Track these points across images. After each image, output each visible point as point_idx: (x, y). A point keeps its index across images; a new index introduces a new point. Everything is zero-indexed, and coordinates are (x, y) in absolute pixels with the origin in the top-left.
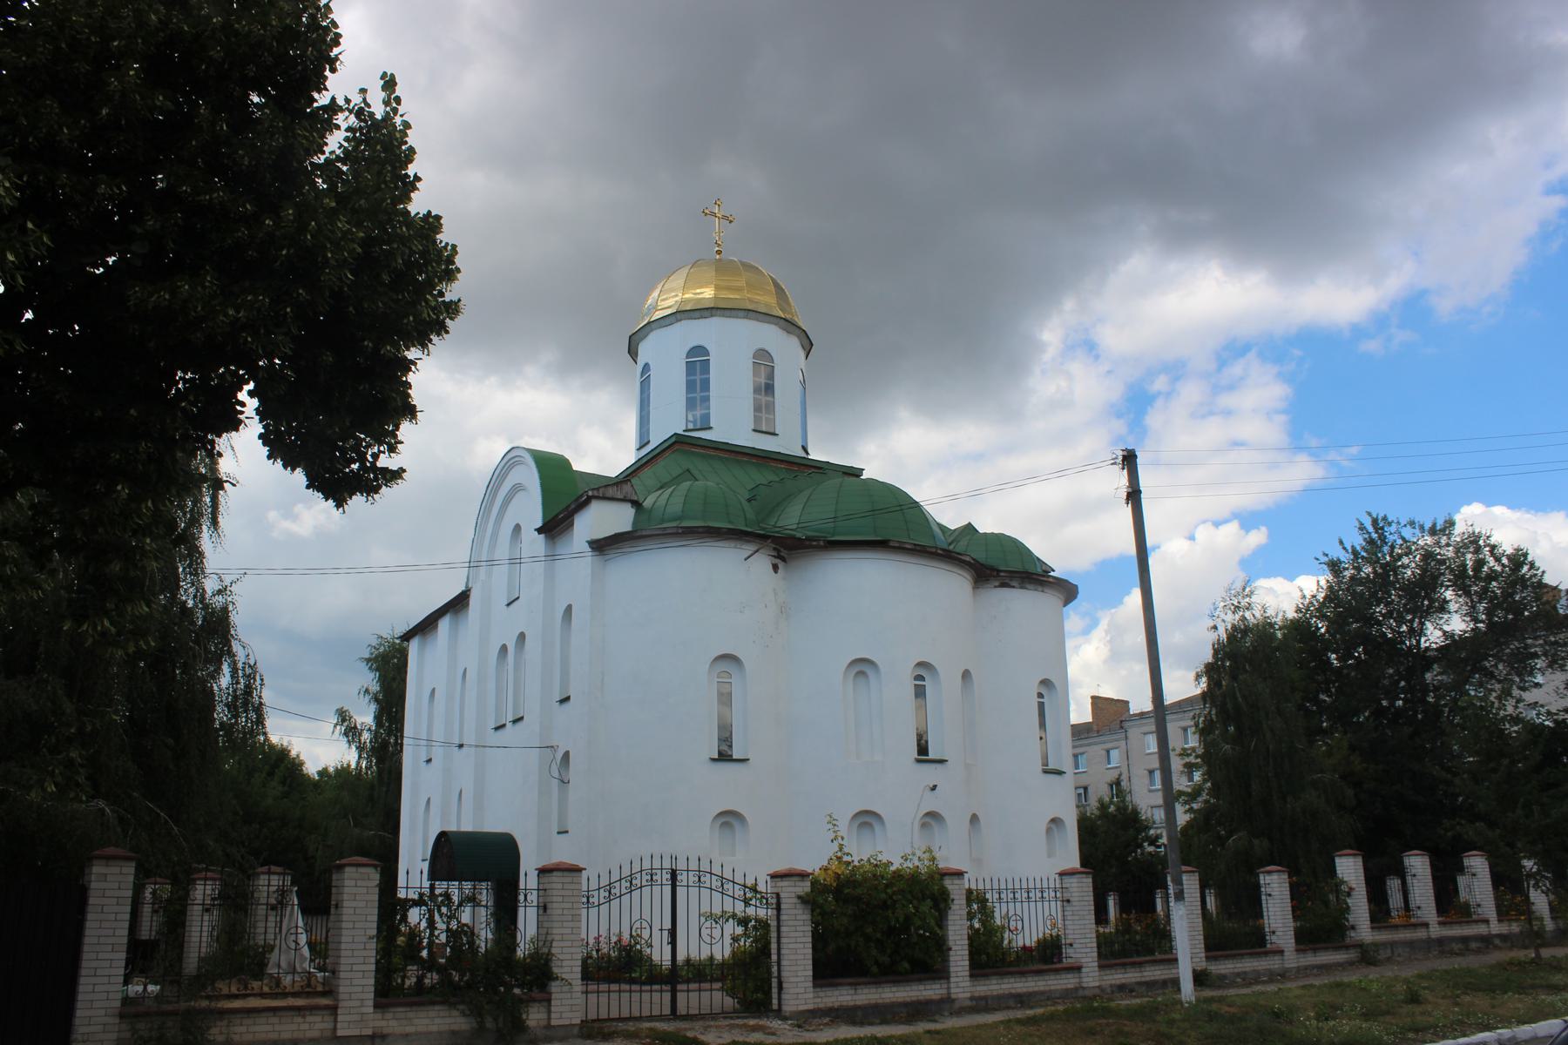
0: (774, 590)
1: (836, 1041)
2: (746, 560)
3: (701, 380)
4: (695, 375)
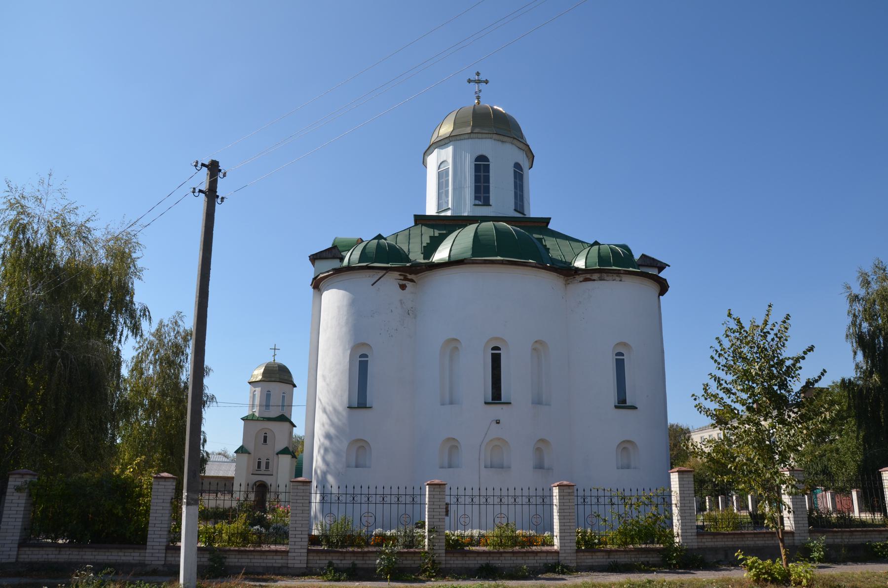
0: (401, 300)
1: (286, 587)
2: (373, 285)
3: (484, 176)
4: (484, 176)
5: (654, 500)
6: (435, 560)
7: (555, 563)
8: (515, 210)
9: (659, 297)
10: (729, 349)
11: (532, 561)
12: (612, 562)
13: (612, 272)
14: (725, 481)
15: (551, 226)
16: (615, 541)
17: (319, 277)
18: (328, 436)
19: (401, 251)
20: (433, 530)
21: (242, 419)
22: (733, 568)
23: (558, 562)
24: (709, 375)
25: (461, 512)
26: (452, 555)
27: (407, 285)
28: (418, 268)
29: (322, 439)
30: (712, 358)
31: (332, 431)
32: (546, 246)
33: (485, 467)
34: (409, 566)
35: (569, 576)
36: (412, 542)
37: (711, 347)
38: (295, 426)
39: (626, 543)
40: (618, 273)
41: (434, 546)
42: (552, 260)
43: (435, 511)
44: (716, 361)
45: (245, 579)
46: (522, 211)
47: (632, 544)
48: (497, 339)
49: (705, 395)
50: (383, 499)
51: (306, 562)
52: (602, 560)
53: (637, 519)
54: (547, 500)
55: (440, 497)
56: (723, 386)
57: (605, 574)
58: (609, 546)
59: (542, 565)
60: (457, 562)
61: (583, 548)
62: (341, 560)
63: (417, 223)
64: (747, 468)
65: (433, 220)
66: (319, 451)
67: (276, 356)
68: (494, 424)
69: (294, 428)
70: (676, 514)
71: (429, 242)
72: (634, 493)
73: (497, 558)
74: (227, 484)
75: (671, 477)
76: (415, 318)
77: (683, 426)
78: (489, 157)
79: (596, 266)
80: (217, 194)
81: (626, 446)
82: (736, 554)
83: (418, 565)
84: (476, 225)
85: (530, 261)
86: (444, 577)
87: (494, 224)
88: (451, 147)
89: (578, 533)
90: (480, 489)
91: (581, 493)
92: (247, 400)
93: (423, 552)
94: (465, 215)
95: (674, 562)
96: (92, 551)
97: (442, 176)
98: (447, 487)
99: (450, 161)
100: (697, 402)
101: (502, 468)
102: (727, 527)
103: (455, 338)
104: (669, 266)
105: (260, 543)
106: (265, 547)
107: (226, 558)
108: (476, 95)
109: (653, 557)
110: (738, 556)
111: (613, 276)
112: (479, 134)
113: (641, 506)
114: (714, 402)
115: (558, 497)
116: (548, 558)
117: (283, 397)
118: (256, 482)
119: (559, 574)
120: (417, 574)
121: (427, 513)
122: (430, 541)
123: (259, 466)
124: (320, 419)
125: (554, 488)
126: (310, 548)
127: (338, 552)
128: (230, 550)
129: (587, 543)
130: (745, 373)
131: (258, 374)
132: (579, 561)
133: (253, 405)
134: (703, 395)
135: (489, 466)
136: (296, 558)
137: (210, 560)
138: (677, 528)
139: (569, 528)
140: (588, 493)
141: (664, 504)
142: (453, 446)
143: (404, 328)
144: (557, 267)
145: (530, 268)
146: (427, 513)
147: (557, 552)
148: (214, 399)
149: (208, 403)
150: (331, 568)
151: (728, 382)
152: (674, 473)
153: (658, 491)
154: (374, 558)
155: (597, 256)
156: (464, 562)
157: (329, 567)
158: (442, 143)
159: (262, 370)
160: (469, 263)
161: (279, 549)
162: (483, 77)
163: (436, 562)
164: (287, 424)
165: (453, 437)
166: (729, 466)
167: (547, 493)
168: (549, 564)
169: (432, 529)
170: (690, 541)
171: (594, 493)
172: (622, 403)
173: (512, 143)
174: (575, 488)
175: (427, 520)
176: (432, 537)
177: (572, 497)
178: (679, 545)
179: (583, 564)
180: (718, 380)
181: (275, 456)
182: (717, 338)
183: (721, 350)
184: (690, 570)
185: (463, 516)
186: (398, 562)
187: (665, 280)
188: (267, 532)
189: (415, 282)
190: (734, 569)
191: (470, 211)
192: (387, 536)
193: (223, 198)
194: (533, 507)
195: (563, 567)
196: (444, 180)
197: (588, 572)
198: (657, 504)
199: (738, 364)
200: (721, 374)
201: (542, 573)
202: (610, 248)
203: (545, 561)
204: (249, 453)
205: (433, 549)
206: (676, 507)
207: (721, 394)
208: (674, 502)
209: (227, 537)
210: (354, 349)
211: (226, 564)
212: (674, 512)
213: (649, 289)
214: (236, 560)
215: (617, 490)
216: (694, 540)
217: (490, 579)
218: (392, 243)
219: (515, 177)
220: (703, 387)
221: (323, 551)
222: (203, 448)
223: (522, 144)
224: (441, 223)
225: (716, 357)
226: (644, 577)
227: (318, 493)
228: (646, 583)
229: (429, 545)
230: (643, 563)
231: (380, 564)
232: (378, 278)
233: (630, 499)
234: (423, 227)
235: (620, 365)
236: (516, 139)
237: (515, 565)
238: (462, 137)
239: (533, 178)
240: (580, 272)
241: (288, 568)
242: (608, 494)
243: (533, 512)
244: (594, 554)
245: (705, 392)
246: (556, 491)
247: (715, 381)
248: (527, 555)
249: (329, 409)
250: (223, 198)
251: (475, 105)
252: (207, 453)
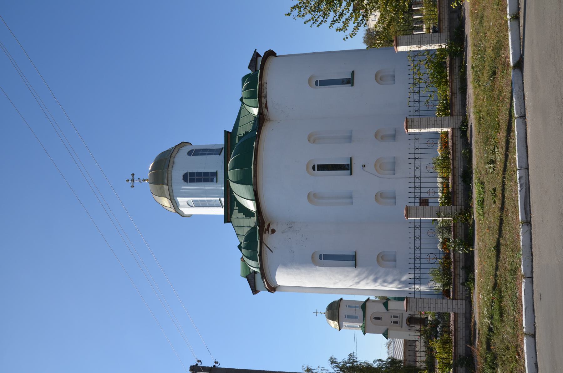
0: (282, 233)
2: (272, 252)
5: (416, 63)
6: (459, 213)
7: (460, 130)
8: (220, 154)
9: (277, 56)
10: (312, 15)
11: (459, 147)
12: (459, 91)
13: (260, 89)
14: (403, 16)
15: (230, 130)
16: (444, 89)
17: (268, 288)
18: (375, 280)
19: (249, 232)
20: (438, 215)
21: (364, 335)
22: (463, 7)
23: (459, 128)
24: (330, 28)
25: (425, 108)
26: (455, 201)
27: (272, 229)
28: (260, 221)
29: (377, 284)
30: (318, 26)
31: (372, 277)
32: (243, 134)
33: (395, 174)
34: (463, 230)
35: (469, 121)
36: (447, 228)
37: (311, 27)
38: (369, 298)
39: (446, 82)
40: (261, 86)
41: (449, 214)
42: (253, 130)
43: (424, 41)
44: (321, 23)
45: (474, 345)
46: (221, 150)
47: (446, 77)
48: (308, 165)
49: (344, 30)
50: (418, 248)
51: (461, 301)
52: (458, 98)
53: (429, 74)
54: (417, 137)
55: (415, 209)
56: (338, 19)
57: (467, 97)
58: (448, 93)
59: (461, 140)
60: (460, 198)
61: (449, 111)
62: (460, 277)
63: (230, 221)
64: (394, 3)
65: (227, 211)
66: (385, 286)
67: (322, 312)
68: (365, 169)
69: (370, 299)
70: (426, 47)
71: (242, 214)
72: (411, 77)
73: (457, 170)
74: (409, 344)
75: (400, 51)
76: (294, 223)
77: (364, 33)
78: (184, 173)
79: (257, 100)
80: (213, 366)
81: (379, 78)
82: (454, 8)
83: (463, 224)
84: (231, 183)
85: (254, 145)
86: (471, 207)
87: (230, 170)
88: (178, 199)
89: (439, 114)
90: (410, 178)
91: (412, 113)
92: (352, 331)
93: (454, 221)
94: (224, 189)
95: (459, 49)
96: (456, 185)
97: (197, 205)
98: (409, 205)
99: (187, 199)
100: (349, 37)
101: (395, 162)
102: (434, 11)
103: (307, 195)
104: (256, 50)
105: (449, 332)
106: (452, 328)
107: (460, 356)
108: (142, 182)
109: (456, 63)
110: (455, 6)
111: (263, 89)
112: (169, 180)
113: (421, 72)
114: (349, 24)
115: (415, 129)
116: (457, 135)
117: (349, 307)
118: (407, 325)
119: (467, 128)
120: (469, 225)
121: (427, 219)
122: (446, 216)
123: (396, 322)
124: (363, 285)
125: (409, 132)
126: (452, 298)
127: (454, 278)
128: (455, 353)
129: (446, 109)
130: (328, 4)
131: (334, 324)
132: (458, 114)
133: (355, 327)
134: (344, 31)
135: (394, 171)
136: (459, 308)
137: (462, 366)
138: (436, 47)
139: (436, 122)
140: (412, 109)
141: (419, 56)
142: (380, 196)
143: (301, 230)
144: (258, 127)
145: (258, 188)
146: (427, 219)
147: (453, 129)
148: (351, 355)
149: (354, 359)
150: (465, 284)
151: (335, 15)
152: (398, 49)
153: (410, 60)
154: (458, 254)
155: (250, 99)
156: (460, 193)
157: (464, 285)
158: (175, 205)
159: (331, 321)
160: (257, 187)
161: (453, 319)
162: (130, 178)
163: (460, 212)
164: (367, 304)
165: (375, 196)
166: (392, 15)
167: (412, 137)
168: (460, 134)
169: (437, 215)
170: (444, 37)
171: (412, 104)
172: (349, 82)
173: (174, 157)
174: (408, 117)
175: (431, 219)
176: (443, 215)
177: (415, 119)
178: (447, 45)
179: (461, 111)
180: (333, 22)
181: (389, 311)
182: (305, 23)
183: (313, 20)
184: (465, 37)
185: (429, 234)
186: (460, 238)
187: (265, 52)
188: (442, 322)
189: (270, 223)
190: (464, 6)
191: (221, 185)
192: (443, 241)
193: (216, 362)
194: (422, 146)
195: (463, 125)
196: (200, 203)
197: (466, 108)
198: (419, 61)
199: (322, 8)
200: (330, 19)
201: (467, 139)
202: (244, 91)
203: (459, 137)
204: (388, 329)
205: (451, 214)
206: (421, 47)
207: (343, 19)
208: (417, 49)
209: (446, 354)
210: (316, 264)
211: (464, 355)
212: (424, 49)
213: (272, 63)
214: (461, 348)
215: (410, 88)
216: (444, 35)
217: (472, 175)
218: (243, 239)
219: (197, 155)
220: (338, 32)
221: (454, 289)
222: (384, 361)
223: (175, 150)
224: (229, 205)
225: (318, 23)
226: (470, 71)
227: (414, 286)
228: (474, 70)
229: (449, 217)
230: (460, 70)
231: (462, 250)
232: (268, 249)
233: (415, 79)
234: (232, 217)
235: (324, 83)
236: (171, 154)
237: (462, 158)
238: (171, 191)
239: (198, 142)
240: (261, 111)
241: (466, 313)
242: (412, 95)
243: (425, 146)
244: (454, 104)
245: (342, 30)
246: (411, 131)
247: (335, 24)
248: (455, 150)
249: (357, 280)
250: (216, 362)
251: (149, 183)
252: (388, 358)
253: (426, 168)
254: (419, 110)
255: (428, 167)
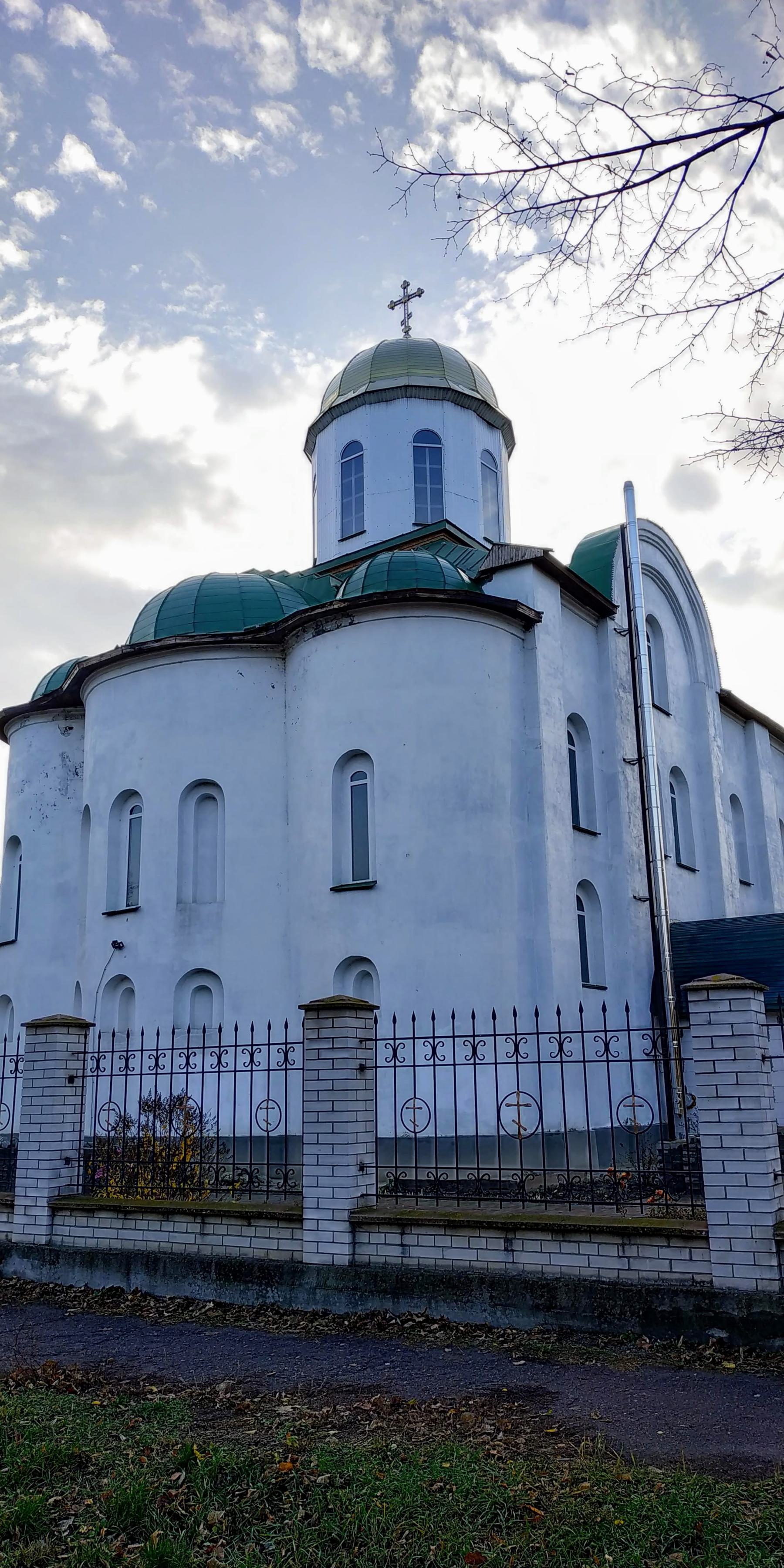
98: (93, 1033)
243: (621, 1089)
253: (518, 1092)
254: (565, 1058)
255: (524, 1099)
